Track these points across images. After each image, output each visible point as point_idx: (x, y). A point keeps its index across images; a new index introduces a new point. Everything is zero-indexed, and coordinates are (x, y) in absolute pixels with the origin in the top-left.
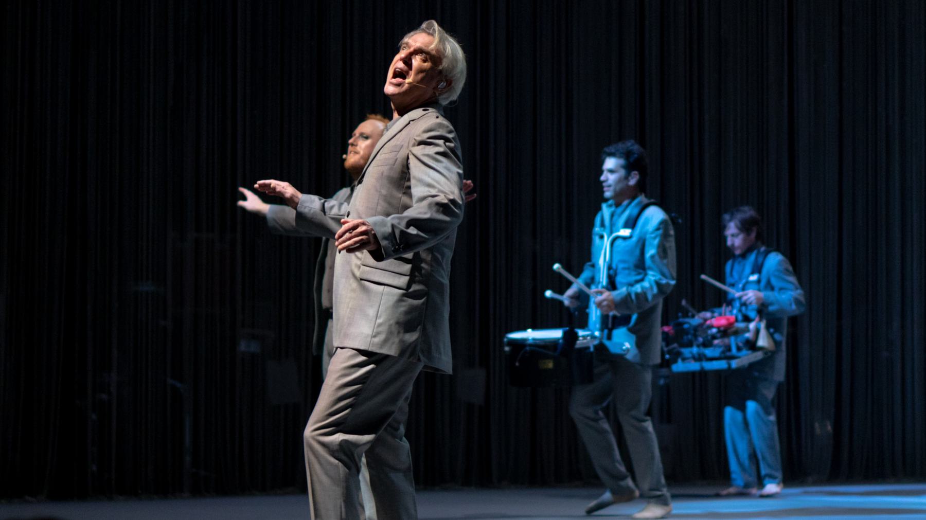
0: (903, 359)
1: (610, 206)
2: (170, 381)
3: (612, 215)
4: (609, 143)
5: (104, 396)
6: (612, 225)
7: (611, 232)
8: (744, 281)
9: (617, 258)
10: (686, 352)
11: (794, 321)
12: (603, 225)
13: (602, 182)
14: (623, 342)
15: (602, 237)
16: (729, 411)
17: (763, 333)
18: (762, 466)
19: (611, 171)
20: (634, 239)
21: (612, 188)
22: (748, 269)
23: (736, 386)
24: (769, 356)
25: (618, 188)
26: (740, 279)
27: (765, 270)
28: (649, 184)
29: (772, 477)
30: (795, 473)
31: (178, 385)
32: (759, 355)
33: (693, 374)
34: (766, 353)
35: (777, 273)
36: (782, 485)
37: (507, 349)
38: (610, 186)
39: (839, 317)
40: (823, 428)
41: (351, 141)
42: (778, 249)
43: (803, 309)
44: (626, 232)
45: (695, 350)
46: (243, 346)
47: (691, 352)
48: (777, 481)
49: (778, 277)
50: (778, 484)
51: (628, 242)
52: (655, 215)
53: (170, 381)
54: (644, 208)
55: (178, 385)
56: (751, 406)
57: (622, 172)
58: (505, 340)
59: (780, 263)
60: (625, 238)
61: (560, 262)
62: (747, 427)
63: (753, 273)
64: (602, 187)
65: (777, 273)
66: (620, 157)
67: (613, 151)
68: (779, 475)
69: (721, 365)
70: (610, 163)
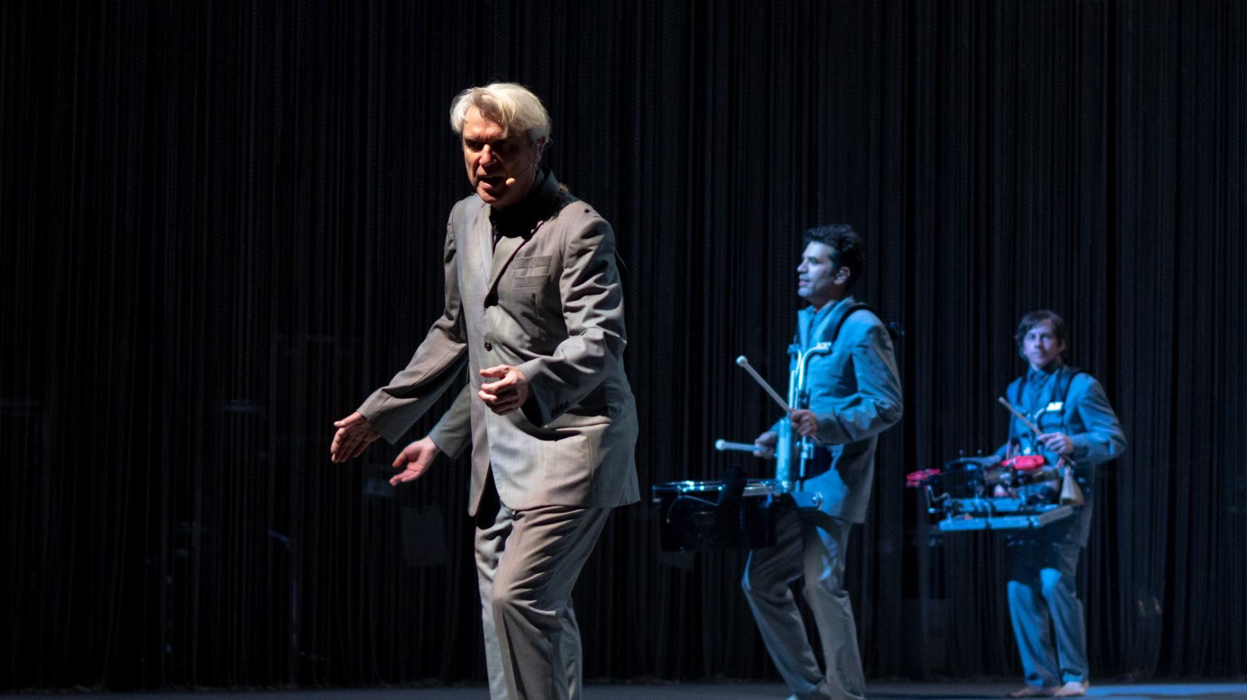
2: (271, 533)
3: (811, 325)
4: (813, 224)
5: (184, 552)
6: (809, 337)
7: (808, 346)
8: (1041, 410)
10: (968, 504)
11: (1111, 466)
13: (798, 274)
14: (823, 492)
15: (796, 357)
16: (1012, 586)
17: (1068, 480)
18: (1061, 656)
19: (815, 261)
20: (835, 354)
21: (811, 284)
22: (1046, 395)
23: (1032, 550)
24: (1079, 509)
25: (819, 285)
26: (1034, 407)
27: (1070, 398)
28: (859, 280)
29: (1075, 673)
30: (1104, 668)
31: (284, 539)
32: (1067, 510)
33: (976, 532)
34: (1075, 509)
35: (1087, 402)
36: (1087, 683)
37: (657, 500)
38: (808, 281)
39: (1173, 459)
40: (1149, 607)
41: (800, 268)
42: (1090, 372)
43: (1123, 449)
44: (824, 346)
45: (977, 501)
47: (973, 504)
48: (1081, 678)
49: (1085, 405)
50: (1083, 682)
52: (864, 320)
53: (271, 533)
54: (850, 311)
55: (284, 539)
56: (1049, 577)
57: (829, 265)
59: (1091, 389)
60: (823, 354)
62: (1039, 606)
63: (1053, 400)
64: (798, 281)
65: (1087, 402)
66: (829, 244)
67: (821, 234)
68: (1085, 671)
69: (1022, 522)
70: (814, 249)
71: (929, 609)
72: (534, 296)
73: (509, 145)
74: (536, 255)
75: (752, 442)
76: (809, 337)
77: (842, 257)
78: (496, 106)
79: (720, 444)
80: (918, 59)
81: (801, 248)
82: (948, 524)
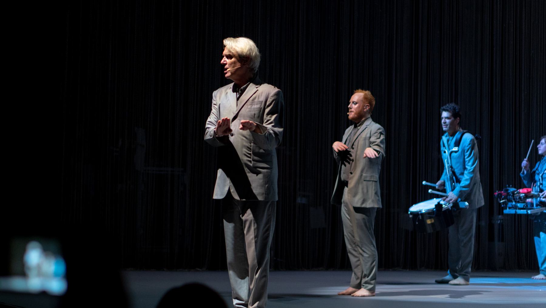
0: (515, 231)
1: (447, 136)
3: (448, 141)
7: (449, 149)
9: (454, 162)
12: (444, 146)
20: (460, 151)
28: (462, 122)
37: (411, 216)
41: (349, 106)
44: (456, 149)
46: (299, 200)
51: (457, 153)
52: (468, 137)
57: (453, 119)
58: (335, 156)
60: (456, 152)
61: (425, 180)
70: (445, 114)
71: (498, 246)
72: (255, 114)
73: (243, 59)
74: (256, 100)
75: (435, 183)
76: (449, 145)
77: (455, 115)
78: (240, 45)
79: (424, 183)
80: (495, 49)
81: (440, 115)
82: (507, 211)
